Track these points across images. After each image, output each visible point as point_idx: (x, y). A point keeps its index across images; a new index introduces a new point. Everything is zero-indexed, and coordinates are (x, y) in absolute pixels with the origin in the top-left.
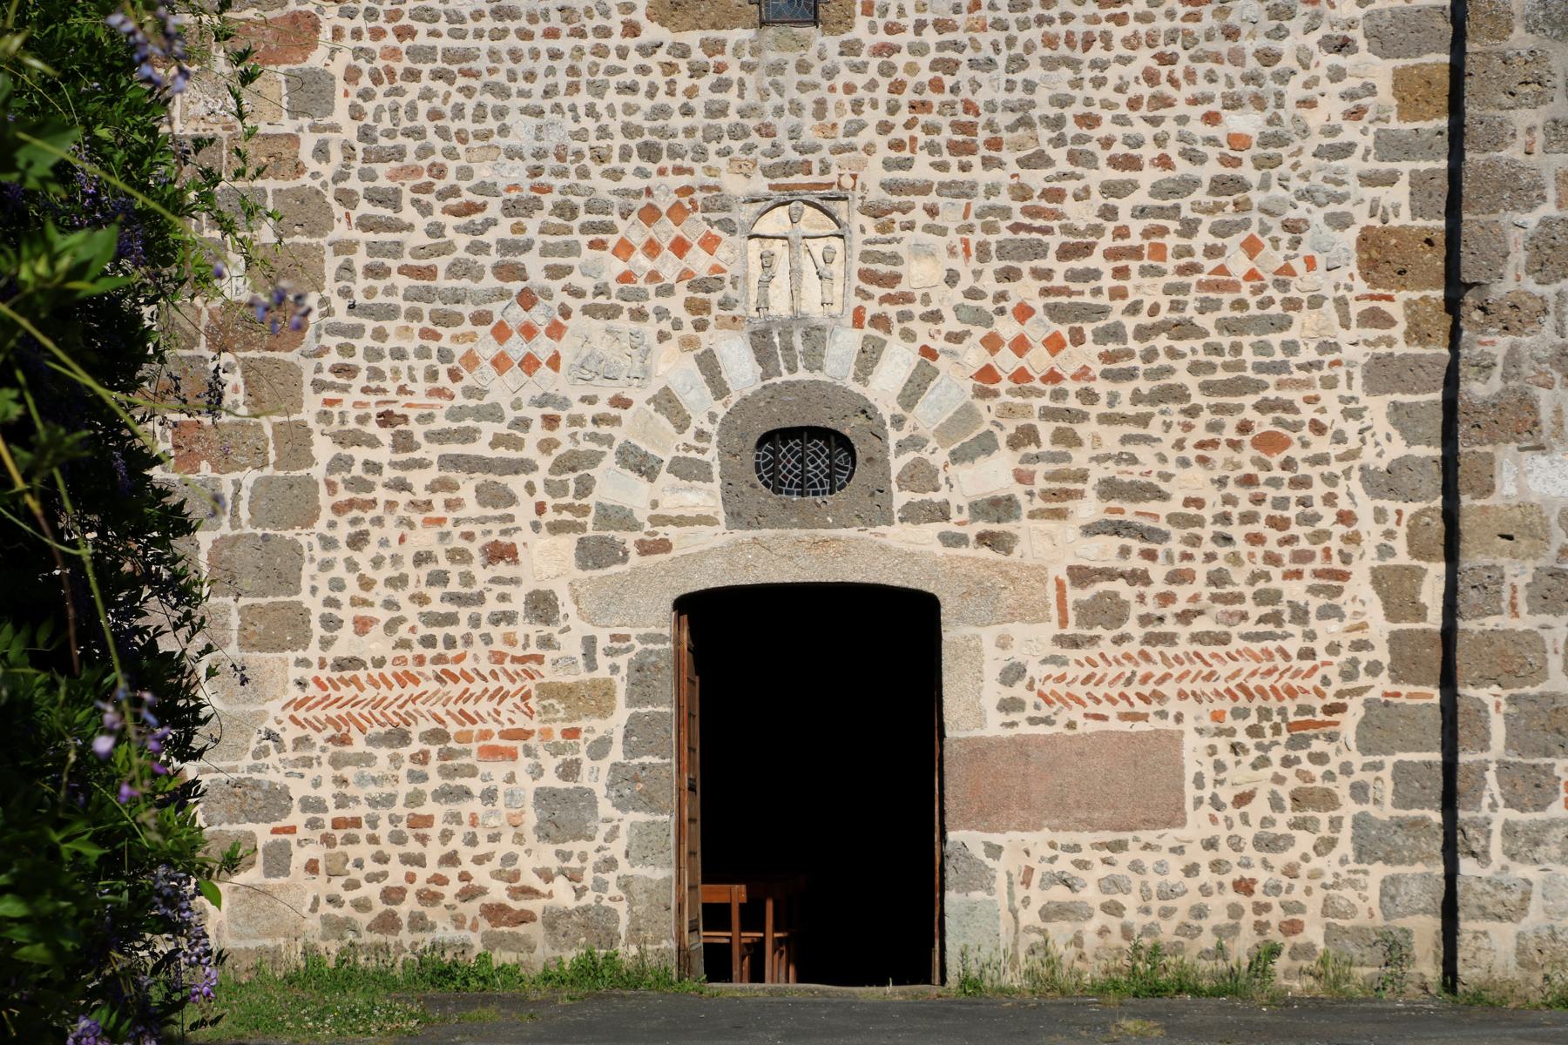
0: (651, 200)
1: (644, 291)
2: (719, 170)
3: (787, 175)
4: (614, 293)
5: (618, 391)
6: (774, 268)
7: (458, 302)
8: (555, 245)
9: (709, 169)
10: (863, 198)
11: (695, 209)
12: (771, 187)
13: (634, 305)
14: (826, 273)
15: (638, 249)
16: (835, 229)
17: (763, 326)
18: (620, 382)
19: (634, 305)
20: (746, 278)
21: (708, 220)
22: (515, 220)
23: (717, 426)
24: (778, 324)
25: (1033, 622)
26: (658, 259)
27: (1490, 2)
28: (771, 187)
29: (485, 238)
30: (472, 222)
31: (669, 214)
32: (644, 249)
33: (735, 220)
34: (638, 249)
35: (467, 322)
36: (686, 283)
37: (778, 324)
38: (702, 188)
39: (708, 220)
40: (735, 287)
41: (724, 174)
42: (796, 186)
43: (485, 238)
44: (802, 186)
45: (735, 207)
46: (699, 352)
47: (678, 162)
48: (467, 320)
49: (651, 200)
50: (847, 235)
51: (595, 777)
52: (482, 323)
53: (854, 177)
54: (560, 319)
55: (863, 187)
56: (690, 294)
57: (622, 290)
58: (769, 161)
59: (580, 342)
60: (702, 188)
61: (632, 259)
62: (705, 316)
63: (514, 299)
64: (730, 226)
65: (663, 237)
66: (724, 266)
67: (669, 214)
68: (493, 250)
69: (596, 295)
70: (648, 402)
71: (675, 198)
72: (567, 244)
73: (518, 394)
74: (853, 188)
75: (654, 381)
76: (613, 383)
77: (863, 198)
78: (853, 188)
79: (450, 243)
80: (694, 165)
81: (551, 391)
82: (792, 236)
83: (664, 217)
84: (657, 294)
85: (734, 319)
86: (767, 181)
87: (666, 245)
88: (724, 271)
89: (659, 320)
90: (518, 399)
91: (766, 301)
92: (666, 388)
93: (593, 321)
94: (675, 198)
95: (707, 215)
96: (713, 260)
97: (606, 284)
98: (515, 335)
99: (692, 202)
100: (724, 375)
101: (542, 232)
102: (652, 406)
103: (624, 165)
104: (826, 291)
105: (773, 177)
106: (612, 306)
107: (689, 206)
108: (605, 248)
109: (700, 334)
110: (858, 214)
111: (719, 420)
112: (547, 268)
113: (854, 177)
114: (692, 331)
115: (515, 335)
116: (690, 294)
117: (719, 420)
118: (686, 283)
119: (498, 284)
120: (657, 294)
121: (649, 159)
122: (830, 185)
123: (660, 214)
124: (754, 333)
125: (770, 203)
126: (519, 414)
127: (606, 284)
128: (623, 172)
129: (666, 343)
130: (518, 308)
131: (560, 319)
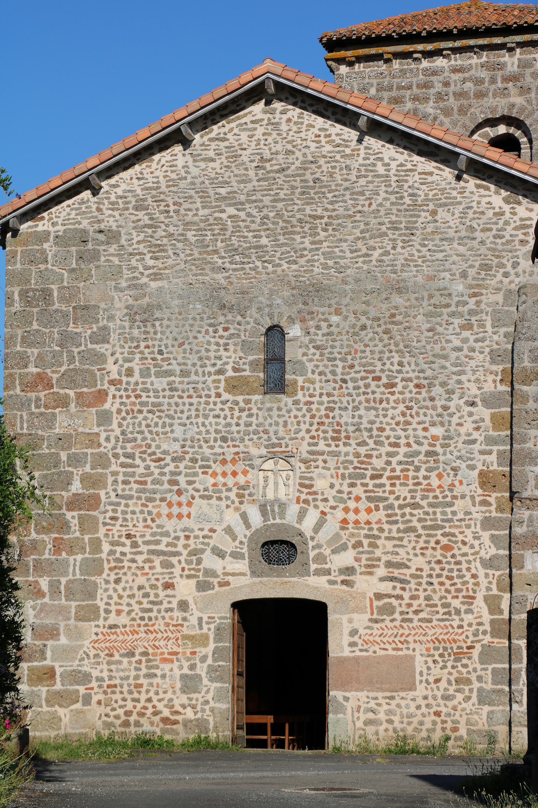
13: (217, 495)
19: (217, 495)
87: (229, 473)
94: (233, 456)
112: (187, 481)
119: (169, 487)
126: (176, 534)
130: (176, 496)
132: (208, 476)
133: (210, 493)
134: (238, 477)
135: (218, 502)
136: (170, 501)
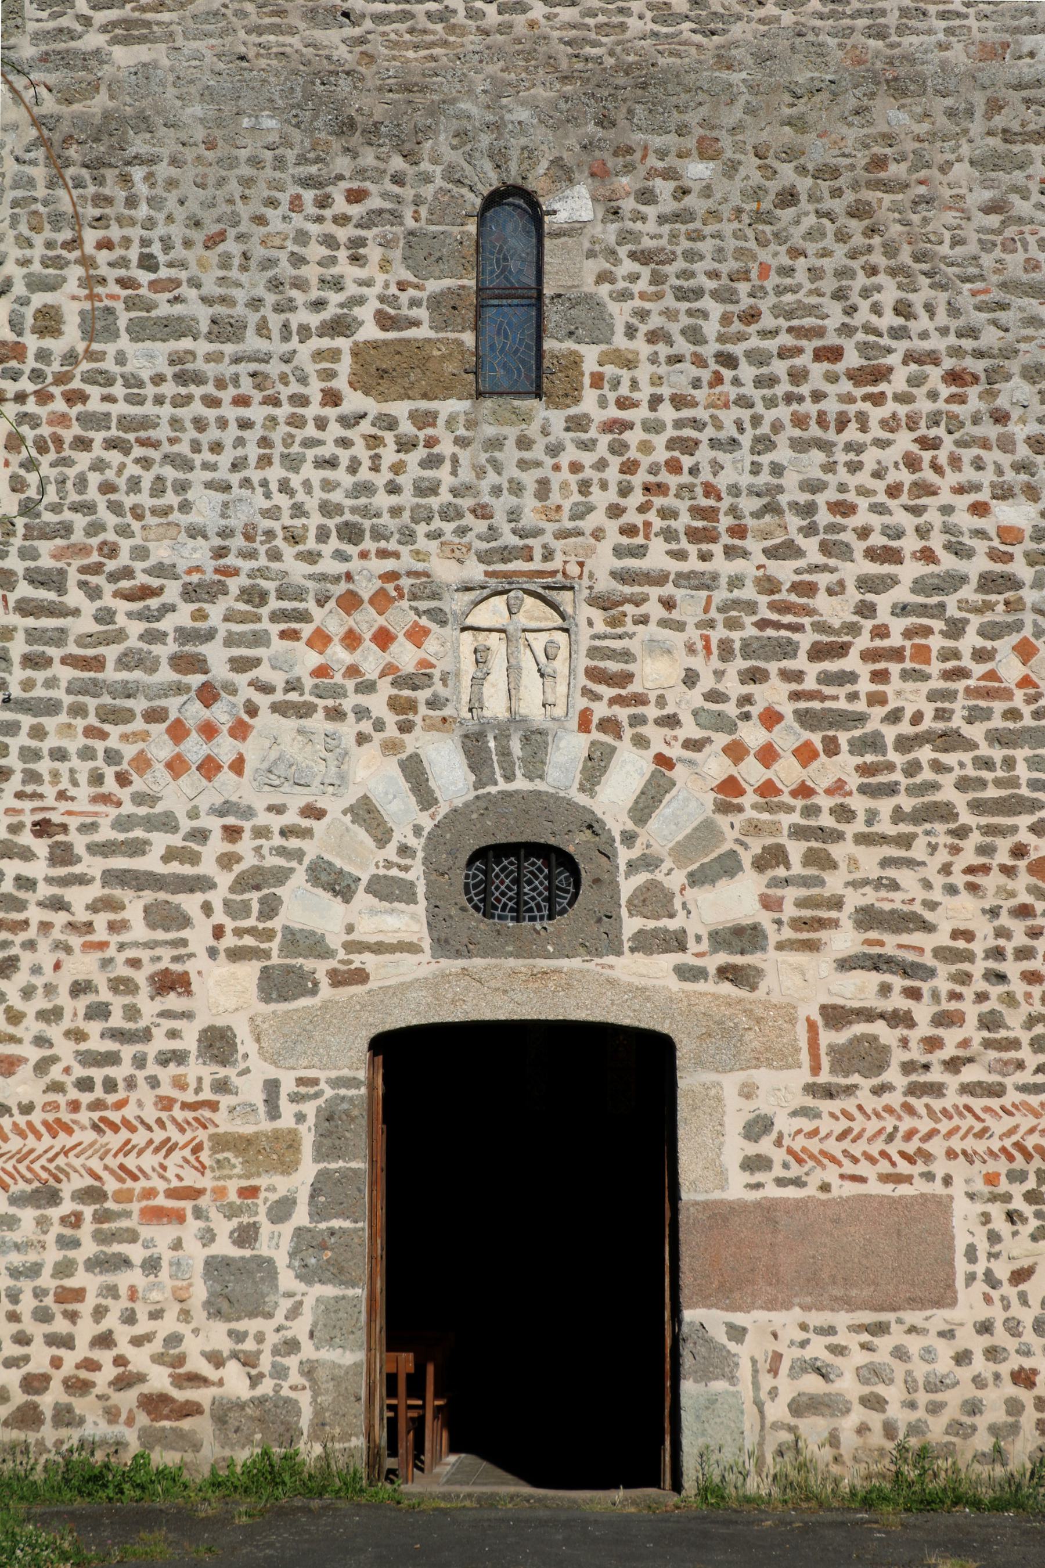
0: (351, 586)
1: (342, 687)
2: (428, 554)
3: (504, 561)
4: (307, 690)
5: (310, 799)
6: (490, 664)
7: (129, 696)
9: (417, 552)
10: (591, 588)
11: (401, 596)
12: (487, 574)
14: (548, 670)
15: (336, 640)
16: (559, 622)
17: (477, 728)
19: (330, 703)
20: (457, 675)
21: (416, 610)
22: (196, 606)
23: (423, 840)
24: (494, 727)
26: (359, 651)
28: (487, 574)
30: (147, 607)
31: (372, 601)
32: (342, 640)
33: (447, 610)
34: (336, 640)
36: (389, 679)
37: (494, 727)
38: (409, 574)
39: (416, 610)
40: (445, 685)
41: (434, 559)
42: (515, 573)
44: (522, 574)
45: (446, 596)
46: (404, 756)
47: (383, 544)
48: (139, 717)
49: (351, 586)
50: (573, 629)
53: (581, 564)
54: (246, 718)
55: (591, 576)
56: (395, 691)
58: (485, 546)
60: (409, 574)
61: (329, 651)
62: (411, 717)
63: (193, 694)
64: (441, 617)
65: (364, 627)
66: (433, 661)
67: (372, 601)
68: (170, 639)
69: (287, 691)
70: (345, 813)
71: (379, 584)
74: (580, 577)
77: (591, 588)
78: (580, 577)
80: (402, 549)
81: (234, 799)
82: (510, 629)
83: (366, 605)
84: (356, 691)
85: (444, 720)
86: (483, 567)
88: (433, 666)
89: (359, 720)
91: (480, 700)
92: (365, 797)
94: (379, 584)
95: (414, 604)
96: (420, 654)
97: (299, 679)
98: (194, 734)
99: (397, 588)
100: (431, 783)
101: (226, 619)
102: (349, 817)
103: (321, 547)
104: (548, 690)
105: (489, 563)
107: (394, 594)
108: (298, 639)
109: (405, 737)
110: (584, 605)
111: (425, 833)
112: (232, 660)
113: (581, 564)
114: (396, 733)
115: (194, 734)
116: (395, 691)
117: (425, 833)
118: (389, 679)
119: (176, 677)
120: (356, 691)
121: (350, 541)
122: (553, 574)
123: (362, 602)
124: (466, 736)
125: (486, 592)
127: (299, 679)
128: (319, 555)
129: (366, 746)
130: (198, 705)
131: (246, 718)
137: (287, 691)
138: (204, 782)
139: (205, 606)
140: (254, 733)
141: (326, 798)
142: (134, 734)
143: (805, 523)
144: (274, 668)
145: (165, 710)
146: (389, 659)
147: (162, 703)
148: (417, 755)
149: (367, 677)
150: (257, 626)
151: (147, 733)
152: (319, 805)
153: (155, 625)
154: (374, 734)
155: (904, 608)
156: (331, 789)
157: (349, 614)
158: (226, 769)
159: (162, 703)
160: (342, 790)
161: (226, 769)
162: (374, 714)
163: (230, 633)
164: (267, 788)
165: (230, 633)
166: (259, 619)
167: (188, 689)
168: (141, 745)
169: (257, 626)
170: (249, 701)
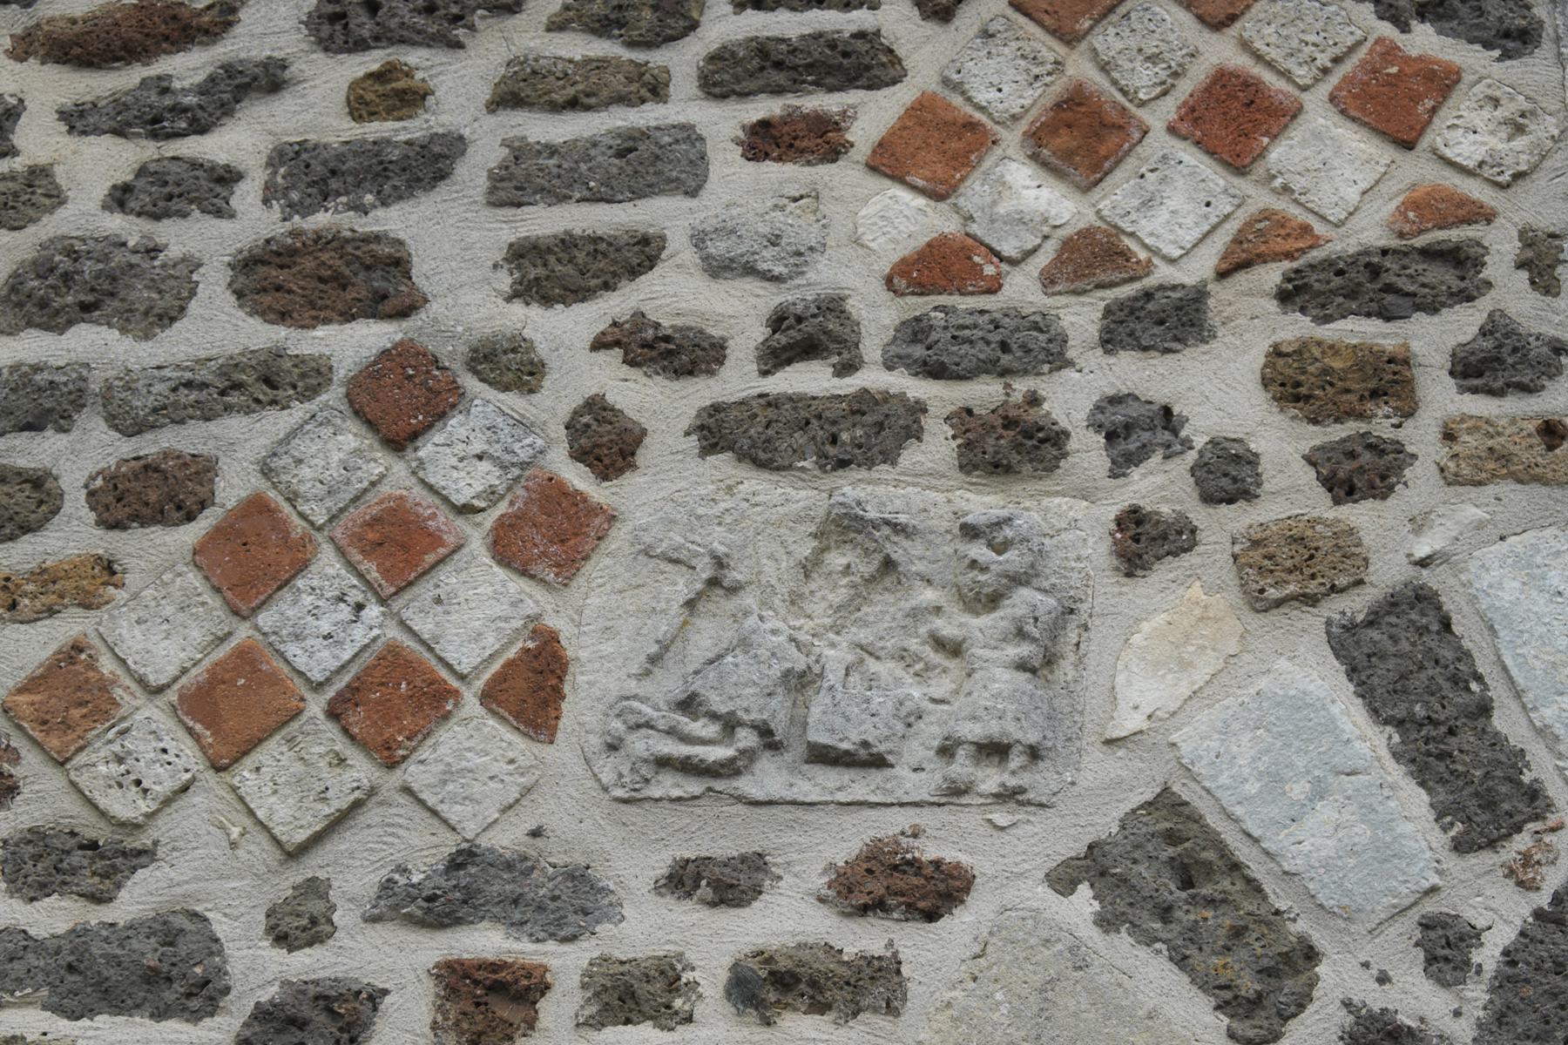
1: (1040, 324)
4: (871, 348)
5: (890, 824)
7: (33, 426)
8: (584, 150)
13: (984, 393)
18: (907, 781)
19: (984, 393)
22: (373, 61)
23: (1477, 994)
25: (1332, 647)
27: (1, 289)
29: (216, 147)
30: (162, 85)
34: (1011, 139)
35: (77, 513)
43: (216, 147)
46: (1355, 605)
48: (76, 505)
51: (558, 996)
52: (156, 516)
54: (577, 477)
56: (1296, 327)
57: (915, 330)
59: (681, 586)
61: (974, 193)
62: (1382, 426)
63: (333, 396)
65: (1143, 78)
66: (1475, 190)
68: (246, 196)
69: (775, 358)
70: (1063, 880)
72: (627, 145)
73: (313, 866)
75: (1097, 767)
76: (861, 786)
79: (39, 174)
81: (506, 839)
84: (1109, 342)
88: (1484, 215)
89: (1122, 464)
90: (315, 888)
92: (1166, 803)
93: (756, 483)
96: (1416, 171)
97: (833, 306)
98: (328, 566)
100: (1506, 721)
101: (508, 98)
102: (1084, 901)
106: (864, 402)
108: (834, 152)
109: (1361, 515)
111: (1488, 956)
112: (520, 253)
114: (1318, 505)
115: (328, 566)
117: (1488, 956)
118: (1272, 275)
119: (259, 335)
120: (1109, 342)
126: (308, 964)
127: (833, 306)
129: (1165, 572)
130: (352, 437)
131: (577, 477)
132: (843, 177)
133: (873, 378)
134: (1283, 154)
135: (982, 503)
136: (256, 506)
137: (775, 358)
138: (362, 770)
139: (413, 57)
140: (619, 538)
141: (969, 819)
142: (45, 577)
143: (162, 256)
144: (718, 269)
145: (203, 470)
146: (1260, 199)
147: (188, 439)
148: (1423, 598)
149: (1163, 273)
150: (647, 116)
151: (109, 569)
152: (929, 851)
153: (191, 147)
154: (1200, 515)
155: (1120, 403)
156: (991, 779)
157: (1070, 39)
158: (471, 703)
159: (188, 439)
160: (1040, 781)
161: (471, 703)
162: (1200, 427)
163: (519, 151)
164: (669, 785)
165: (519, 151)
166: (656, 90)
167: (313, 377)
168: (70, 626)
169: (647, 116)
170: (596, 407)
